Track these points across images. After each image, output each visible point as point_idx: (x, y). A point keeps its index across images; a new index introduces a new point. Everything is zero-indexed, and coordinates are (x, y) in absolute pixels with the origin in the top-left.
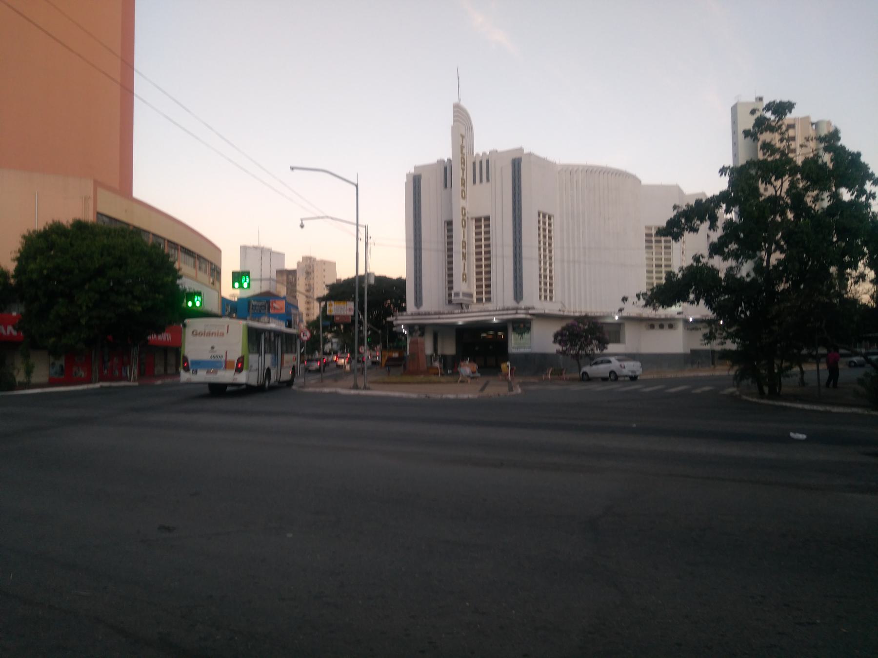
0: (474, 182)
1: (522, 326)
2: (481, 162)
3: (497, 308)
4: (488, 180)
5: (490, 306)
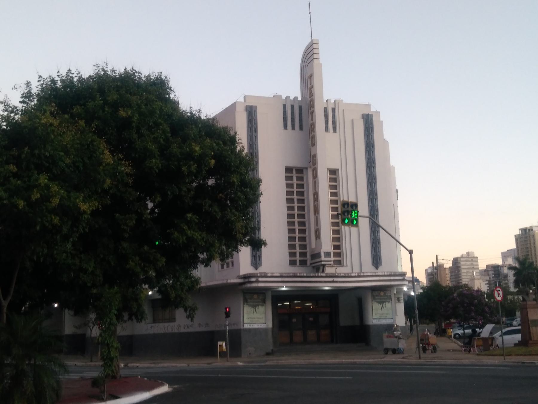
0: (327, 130)
1: (381, 293)
2: (292, 107)
3: (353, 268)
4: (335, 130)
5: (341, 270)
